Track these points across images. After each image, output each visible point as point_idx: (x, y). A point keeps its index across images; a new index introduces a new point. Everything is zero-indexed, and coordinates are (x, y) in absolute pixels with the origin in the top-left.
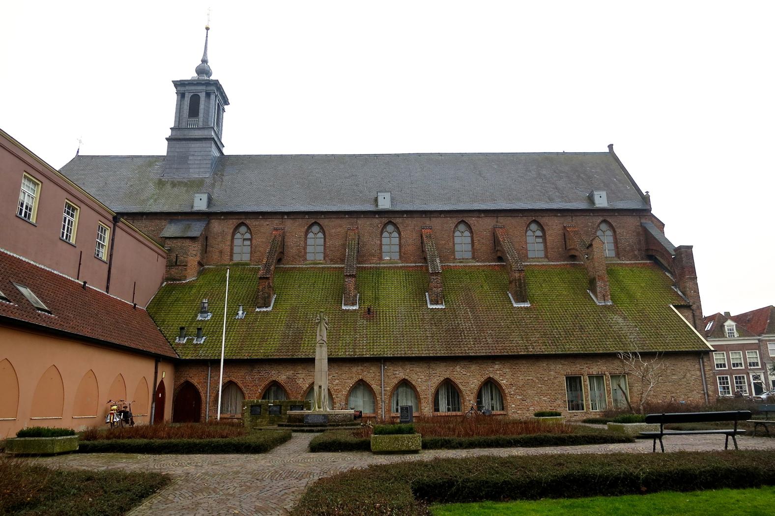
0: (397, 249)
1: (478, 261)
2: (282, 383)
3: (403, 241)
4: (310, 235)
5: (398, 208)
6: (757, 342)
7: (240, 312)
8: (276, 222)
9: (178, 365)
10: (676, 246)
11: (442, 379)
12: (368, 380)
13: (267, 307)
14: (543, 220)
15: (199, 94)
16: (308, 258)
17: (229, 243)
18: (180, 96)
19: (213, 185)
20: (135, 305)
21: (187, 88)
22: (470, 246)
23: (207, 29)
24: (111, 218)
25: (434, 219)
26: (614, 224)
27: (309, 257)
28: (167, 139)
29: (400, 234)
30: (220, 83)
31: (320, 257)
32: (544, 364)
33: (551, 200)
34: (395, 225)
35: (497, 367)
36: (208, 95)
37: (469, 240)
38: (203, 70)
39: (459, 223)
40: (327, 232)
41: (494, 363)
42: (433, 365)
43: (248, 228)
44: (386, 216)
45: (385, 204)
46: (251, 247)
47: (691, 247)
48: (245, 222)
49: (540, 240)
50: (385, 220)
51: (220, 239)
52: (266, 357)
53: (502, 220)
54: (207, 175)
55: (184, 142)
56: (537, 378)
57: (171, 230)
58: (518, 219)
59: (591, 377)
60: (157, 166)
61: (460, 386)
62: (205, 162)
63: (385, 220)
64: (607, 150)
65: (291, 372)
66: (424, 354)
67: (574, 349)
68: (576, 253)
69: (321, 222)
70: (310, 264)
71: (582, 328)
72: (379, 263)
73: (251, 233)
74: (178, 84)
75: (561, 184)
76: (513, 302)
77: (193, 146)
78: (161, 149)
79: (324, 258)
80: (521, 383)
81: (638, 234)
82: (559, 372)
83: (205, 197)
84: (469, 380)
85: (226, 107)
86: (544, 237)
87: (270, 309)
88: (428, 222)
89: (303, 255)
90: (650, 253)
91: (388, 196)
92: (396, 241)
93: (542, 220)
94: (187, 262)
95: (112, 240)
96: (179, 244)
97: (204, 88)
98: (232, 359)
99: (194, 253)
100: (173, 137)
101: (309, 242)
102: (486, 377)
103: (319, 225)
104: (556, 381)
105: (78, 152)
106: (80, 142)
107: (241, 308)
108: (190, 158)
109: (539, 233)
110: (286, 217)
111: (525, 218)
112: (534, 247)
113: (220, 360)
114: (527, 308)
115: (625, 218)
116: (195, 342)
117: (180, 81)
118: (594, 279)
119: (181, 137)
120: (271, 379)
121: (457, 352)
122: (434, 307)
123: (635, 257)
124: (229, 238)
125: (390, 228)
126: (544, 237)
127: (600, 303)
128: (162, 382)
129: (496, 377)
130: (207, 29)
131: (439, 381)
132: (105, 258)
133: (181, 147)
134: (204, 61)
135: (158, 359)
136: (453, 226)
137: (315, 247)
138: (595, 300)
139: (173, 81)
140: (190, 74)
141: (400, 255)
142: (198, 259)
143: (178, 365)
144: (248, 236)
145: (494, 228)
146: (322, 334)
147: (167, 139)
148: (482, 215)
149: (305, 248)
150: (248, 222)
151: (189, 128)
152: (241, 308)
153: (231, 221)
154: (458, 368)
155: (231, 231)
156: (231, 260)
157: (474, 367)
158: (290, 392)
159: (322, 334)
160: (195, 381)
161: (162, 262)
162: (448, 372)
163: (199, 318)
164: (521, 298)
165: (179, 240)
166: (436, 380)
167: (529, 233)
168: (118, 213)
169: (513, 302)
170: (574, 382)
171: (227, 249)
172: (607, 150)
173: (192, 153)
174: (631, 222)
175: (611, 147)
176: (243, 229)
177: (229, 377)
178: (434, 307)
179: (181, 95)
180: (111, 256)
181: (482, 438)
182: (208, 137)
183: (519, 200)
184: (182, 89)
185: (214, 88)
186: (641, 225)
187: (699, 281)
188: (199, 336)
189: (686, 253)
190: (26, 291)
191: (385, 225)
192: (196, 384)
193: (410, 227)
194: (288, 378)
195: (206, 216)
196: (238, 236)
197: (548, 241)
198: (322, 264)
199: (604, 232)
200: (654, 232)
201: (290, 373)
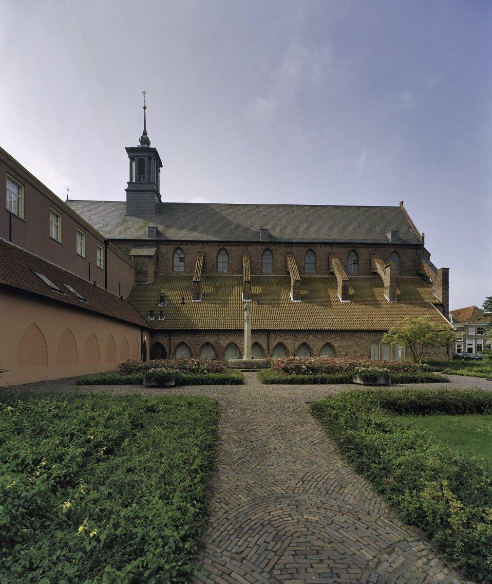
1: (318, 275)
4: (220, 256)
6: (463, 326)
8: (199, 247)
9: (152, 332)
11: (301, 342)
12: (260, 342)
13: (198, 300)
20: (122, 297)
23: (145, 108)
24: (103, 242)
27: (220, 270)
28: (125, 190)
29: (273, 257)
36: (150, 159)
38: (145, 140)
39: (266, 250)
43: (182, 251)
44: (265, 245)
50: (264, 248)
56: (355, 343)
61: (312, 347)
63: (264, 248)
69: (226, 248)
72: (261, 274)
79: (228, 270)
80: (345, 345)
87: (200, 301)
88: (290, 249)
90: (420, 272)
93: (358, 250)
99: (151, 266)
100: (130, 189)
101: (219, 260)
103: (270, 250)
105: (68, 197)
106: (68, 190)
110: (205, 244)
116: (159, 319)
120: (206, 341)
123: (411, 275)
125: (310, 253)
128: (145, 342)
129: (332, 342)
130: (145, 108)
132: (102, 267)
134: (145, 133)
135: (143, 329)
139: (126, 148)
140: (136, 144)
141: (273, 270)
143: (152, 332)
144: (182, 256)
147: (125, 190)
149: (217, 264)
150: (182, 247)
153: (171, 246)
154: (311, 337)
156: (173, 271)
157: (320, 336)
161: (133, 271)
162: (305, 339)
167: (349, 258)
174: (411, 252)
176: (179, 251)
179: (132, 159)
187: (450, 290)
188: (161, 316)
190: (69, 287)
191: (265, 251)
196: (176, 255)
201: (216, 338)
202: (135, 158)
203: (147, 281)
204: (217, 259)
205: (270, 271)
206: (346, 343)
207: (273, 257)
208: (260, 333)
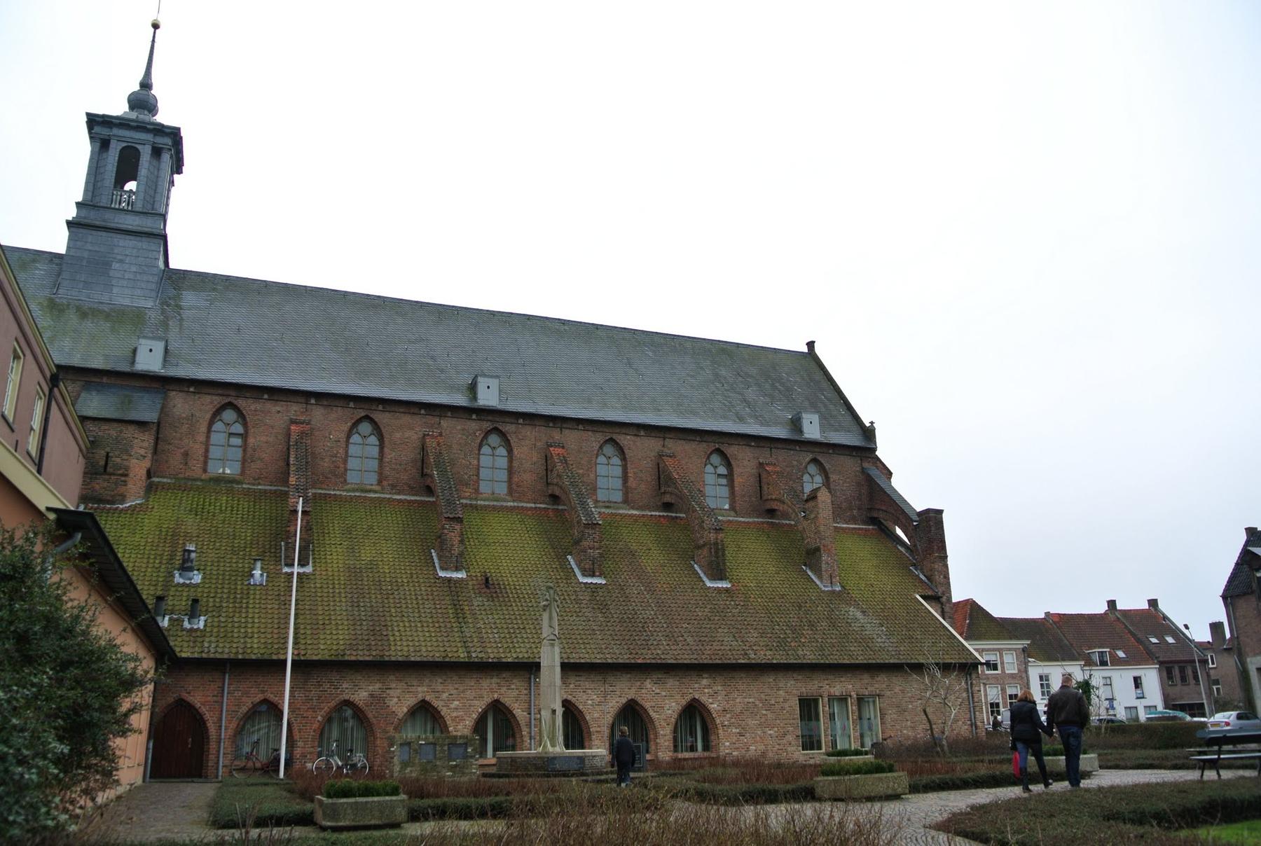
0: (503, 476)
1: (633, 508)
2: (361, 704)
3: (515, 464)
4: (355, 438)
5: (512, 406)
7: (257, 573)
8: (294, 409)
10: (919, 507)
11: (624, 701)
14: (731, 451)
15: (139, 147)
16: (349, 479)
17: (202, 438)
18: (98, 145)
19: (165, 324)
21: (115, 131)
22: (620, 482)
23: (156, 26)
24: (48, 375)
25: (566, 432)
26: (827, 466)
27: (352, 478)
29: (510, 451)
30: (182, 134)
31: (372, 479)
32: (770, 679)
33: (741, 419)
34: (503, 435)
35: (705, 682)
37: (618, 471)
38: (143, 100)
39: (606, 442)
40: (386, 436)
41: (700, 676)
42: (611, 679)
45: (488, 397)
46: (244, 451)
47: (941, 512)
48: (235, 402)
49: (724, 481)
50: (487, 425)
51: (185, 428)
52: (333, 658)
53: (673, 446)
54: (149, 304)
55: (104, 234)
56: (761, 700)
57: (95, 404)
58: (694, 445)
59: (832, 699)
60: (41, 270)
61: (651, 713)
62: (145, 278)
63: (487, 425)
64: (805, 350)
65: (378, 686)
66: (598, 659)
67: (810, 657)
68: (780, 507)
69: (377, 416)
70: (354, 490)
71: (812, 625)
72: (476, 499)
73: (245, 425)
74: (94, 121)
75: (751, 394)
76: (705, 579)
77: (122, 243)
78: (56, 241)
81: (858, 484)
82: (789, 691)
83: (159, 347)
84: (664, 703)
85: (176, 176)
86: (730, 477)
89: (339, 474)
91: (494, 383)
92: (503, 462)
94: (127, 469)
95: (46, 420)
96: (113, 433)
97: (149, 137)
98: (202, 658)
99: (142, 452)
101: (352, 450)
102: (689, 698)
104: (786, 705)
107: (259, 564)
108: (115, 265)
109: (722, 470)
110: (313, 401)
111: (704, 445)
112: (608, 474)
113: (285, 661)
114: (727, 590)
115: (842, 458)
117: (104, 116)
118: (818, 549)
119: (97, 223)
121: (646, 657)
122: (589, 580)
123: (853, 520)
124: (204, 429)
126: (730, 477)
127: (825, 587)
129: (704, 699)
130: (156, 26)
131: (620, 705)
133: (94, 241)
134: (146, 85)
136: (596, 446)
137: (362, 459)
138: (818, 583)
140: (118, 107)
142: (147, 464)
145: (660, 456)
146: (549, 625)
148: (642, 433)
149: (345, 462)
151: (123, 210)
152: (259, 564)
153: (208, 399)
155: (208, 416)
156: (205, 471)
157: (672, 682)
158: (374, 721)
159: (549, 625)
160: (197, 699)
163: (178, 579)
164: (719, 574)
165: (115, 425)
166: (615, 704)
168: (59, 367)
169: (705, 579)
170: (808, 707)
171: (198, 450)
172: (805, 350)
173: (119, 257)
174: (850, 465)
175: (811, 345)
177: (263, 692)
178: (589, 580)
180: (42, 450)
181: (936, 777)
182: (155, 231)
183: (694, 413)
184: (103, 131)
185: (168, 141)
186: (863, 471)
188: (193, 615)
189: (932, 519)
192: (198, 705)
193: (528, 443)
194: (372, 696)
195: (161, 383)
196: (218, 426)
197: (736, 483)
198: (376, 492)
199: (812, 477)
200: (881, 482)
201: (376, 687)
202: (113, 143)
203: (123, 499)
204: (347, 446)
205: (502, 489)
206: (739, 701)
207: (510, 451)
208: (626, 677)
